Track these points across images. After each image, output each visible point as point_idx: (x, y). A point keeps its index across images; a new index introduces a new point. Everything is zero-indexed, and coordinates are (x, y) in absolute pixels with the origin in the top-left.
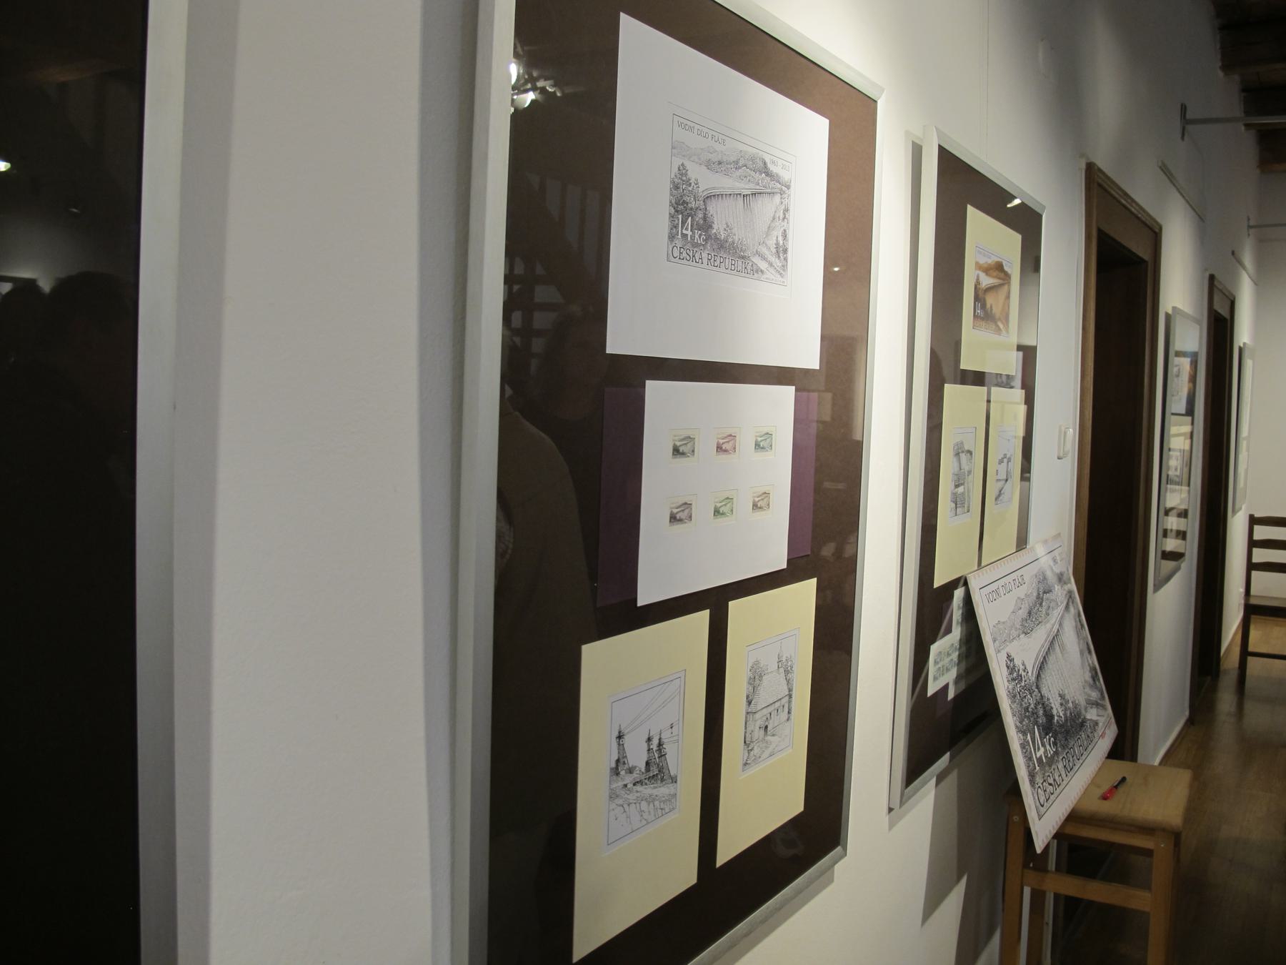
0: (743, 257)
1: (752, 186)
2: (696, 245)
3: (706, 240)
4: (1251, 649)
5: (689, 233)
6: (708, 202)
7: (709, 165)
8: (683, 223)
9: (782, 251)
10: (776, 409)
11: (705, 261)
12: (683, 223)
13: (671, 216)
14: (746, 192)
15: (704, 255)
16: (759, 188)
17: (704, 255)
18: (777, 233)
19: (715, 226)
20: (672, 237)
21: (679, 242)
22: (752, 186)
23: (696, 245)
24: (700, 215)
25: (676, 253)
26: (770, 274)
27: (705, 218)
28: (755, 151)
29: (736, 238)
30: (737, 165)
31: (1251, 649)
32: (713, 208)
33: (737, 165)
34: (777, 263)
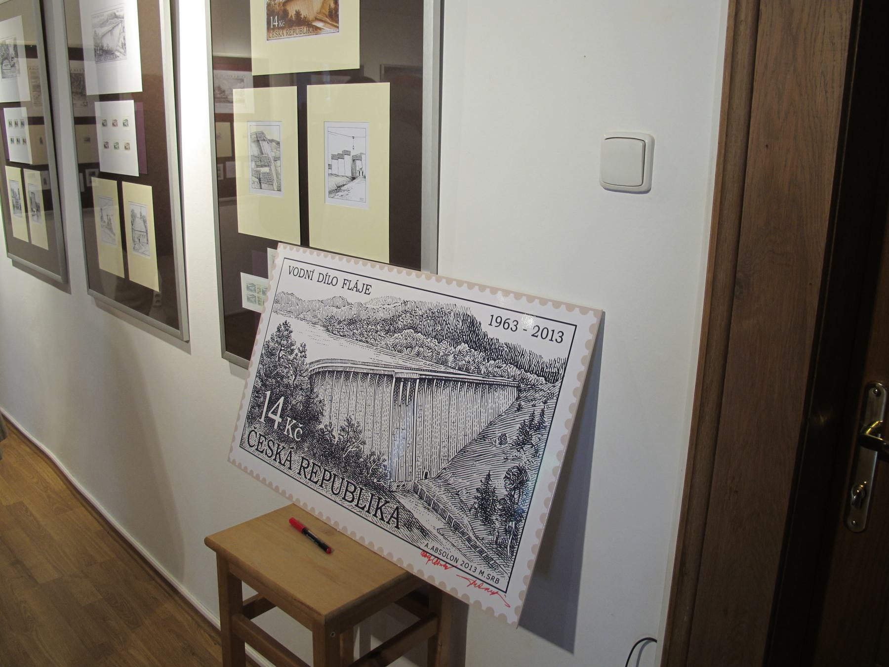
0: (378, 488)
1: (421, 363)
2: (287, 440)
3: (303, 437)
4: (311, 89)
5: (278, 419)
6: (318, 381)
7: (331, 326)
8: (272, 402)
9: (124, 45)
10: (127, 110)
11: (296, 467)
12: (272, 402)
13: (256, 391)
14: (405, 374)
15: (296, 458)
16: (113, 25)
17: (296, 458)
18: (122, 39)
19: (325, 420)
20: (251, 418)
21: (260, 427)
22: (421, 363)
23: (287, 440)
24: (300, 397)
25: (254, 440)
26: (121, 57)
27: (308, 402)
28: (444, 301)
29: (366, 450)
30: (107, 21)
31: (311, 89)
32: (323, 390)
33: (107, 21)
34: (122, 51)
